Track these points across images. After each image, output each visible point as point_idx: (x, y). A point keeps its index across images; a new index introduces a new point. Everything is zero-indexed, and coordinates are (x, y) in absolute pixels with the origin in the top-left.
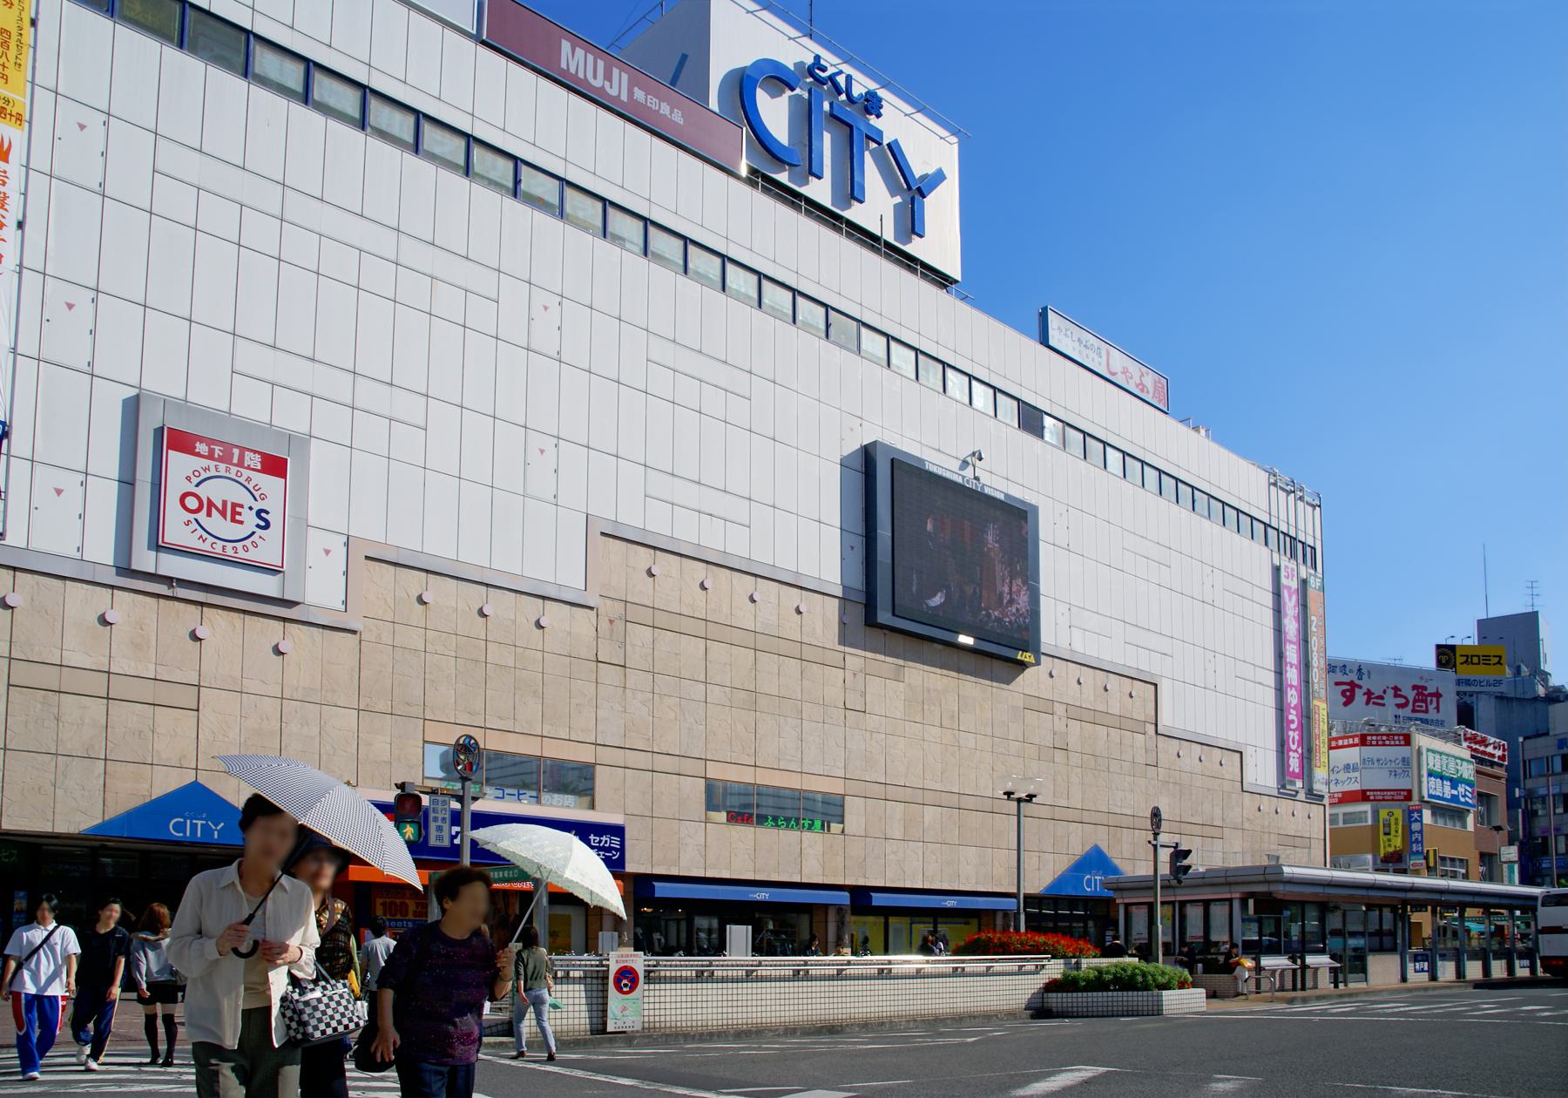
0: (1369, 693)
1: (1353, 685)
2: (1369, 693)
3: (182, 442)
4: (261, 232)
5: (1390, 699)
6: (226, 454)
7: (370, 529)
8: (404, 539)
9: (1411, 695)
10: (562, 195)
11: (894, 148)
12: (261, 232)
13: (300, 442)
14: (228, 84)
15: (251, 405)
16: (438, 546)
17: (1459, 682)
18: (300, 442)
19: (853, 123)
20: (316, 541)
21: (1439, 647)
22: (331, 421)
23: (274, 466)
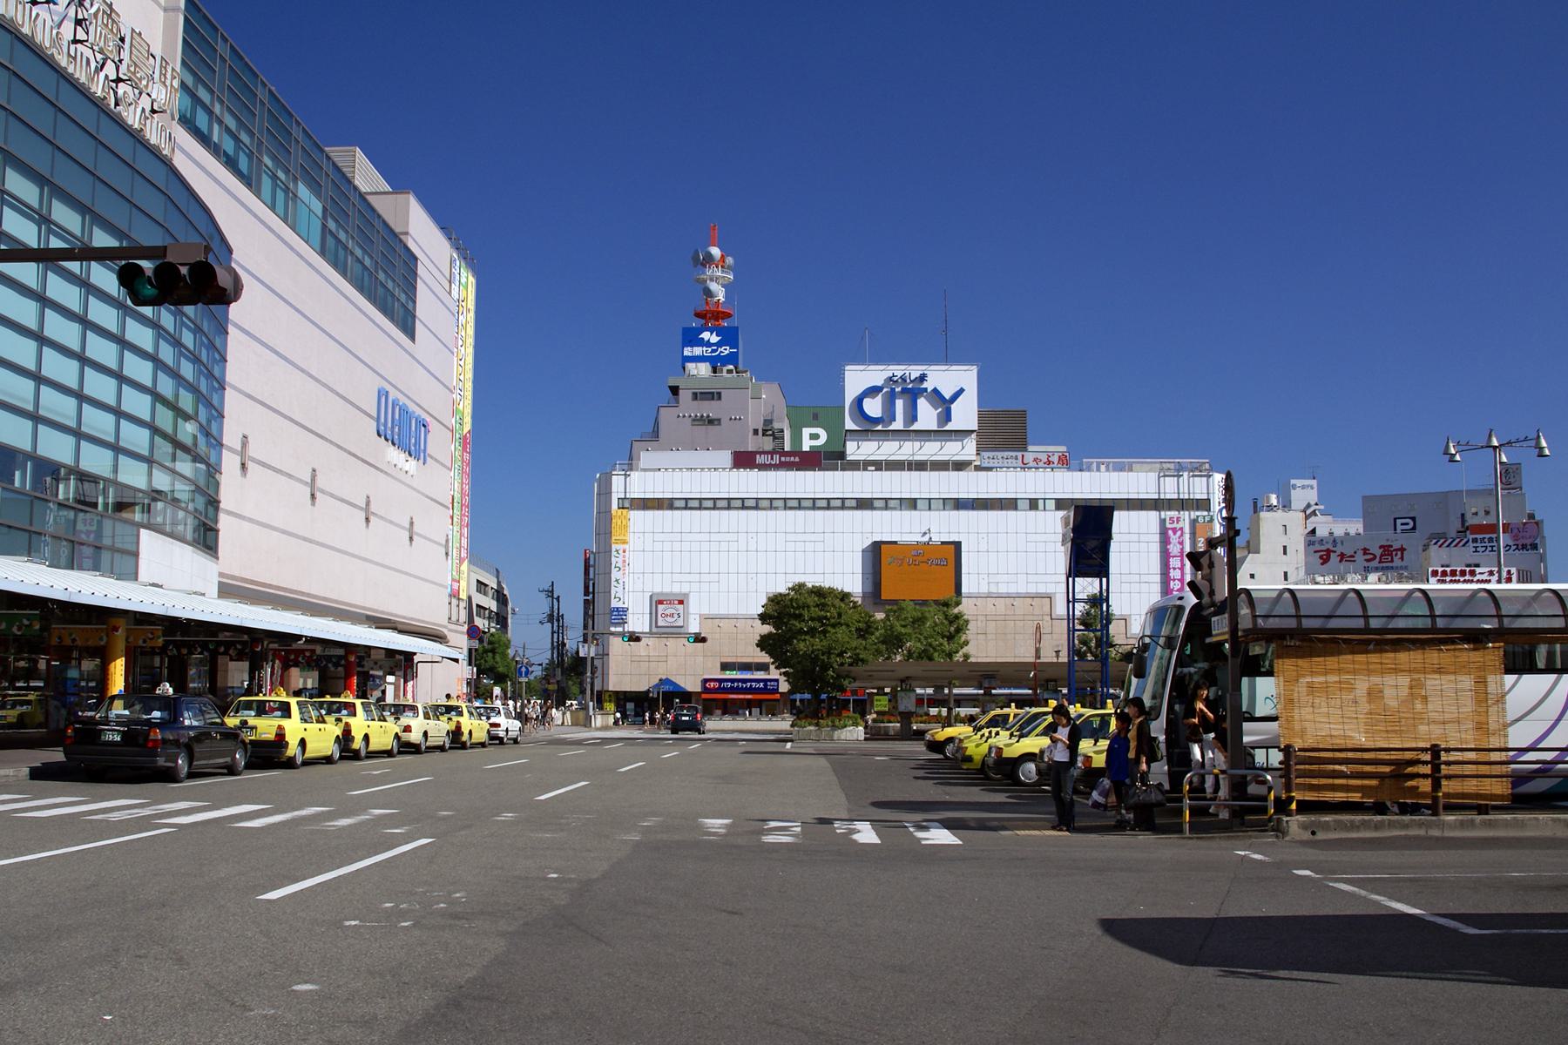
0: (1342, 556)
1: (1329, 552)
2: (1342, 556)
3: (661, 602)
4: (677, 546)
5: (1360, 557)
6: (670, 602)
7: (705, 611)
8: (714, 612)
9: (1378, 552)
10: (1009, 504)
11: (935, 391)
12: (677, 546)
13: (686, 595)
14: (1011, 513)
15: (676, 589)
16: (723, 611)
17: (221, 575)
18: (686, 595)
19: (913, 392)
20: (692, 618)
21: (1364, 498)
22: (695, 587)
23: (681, 602)
